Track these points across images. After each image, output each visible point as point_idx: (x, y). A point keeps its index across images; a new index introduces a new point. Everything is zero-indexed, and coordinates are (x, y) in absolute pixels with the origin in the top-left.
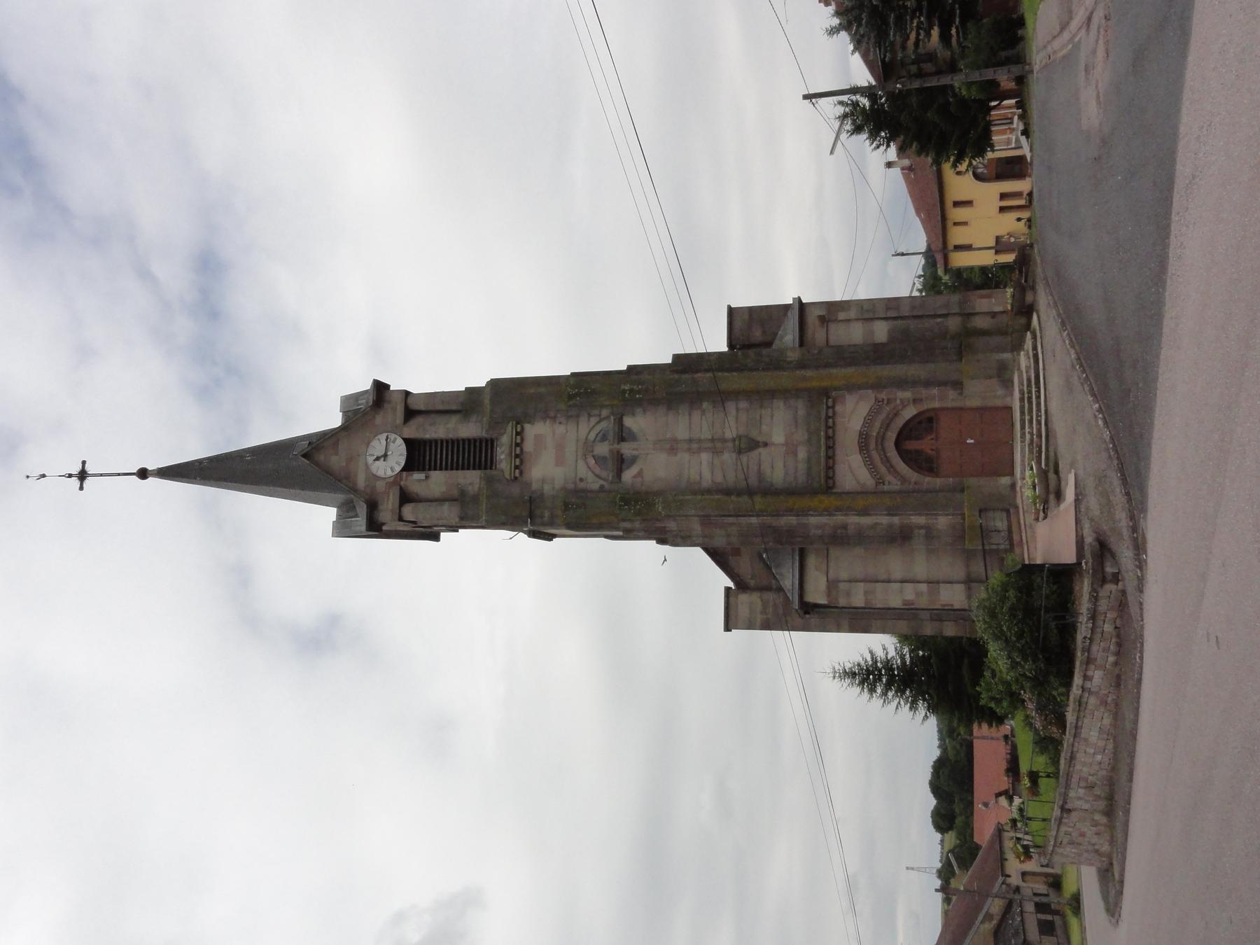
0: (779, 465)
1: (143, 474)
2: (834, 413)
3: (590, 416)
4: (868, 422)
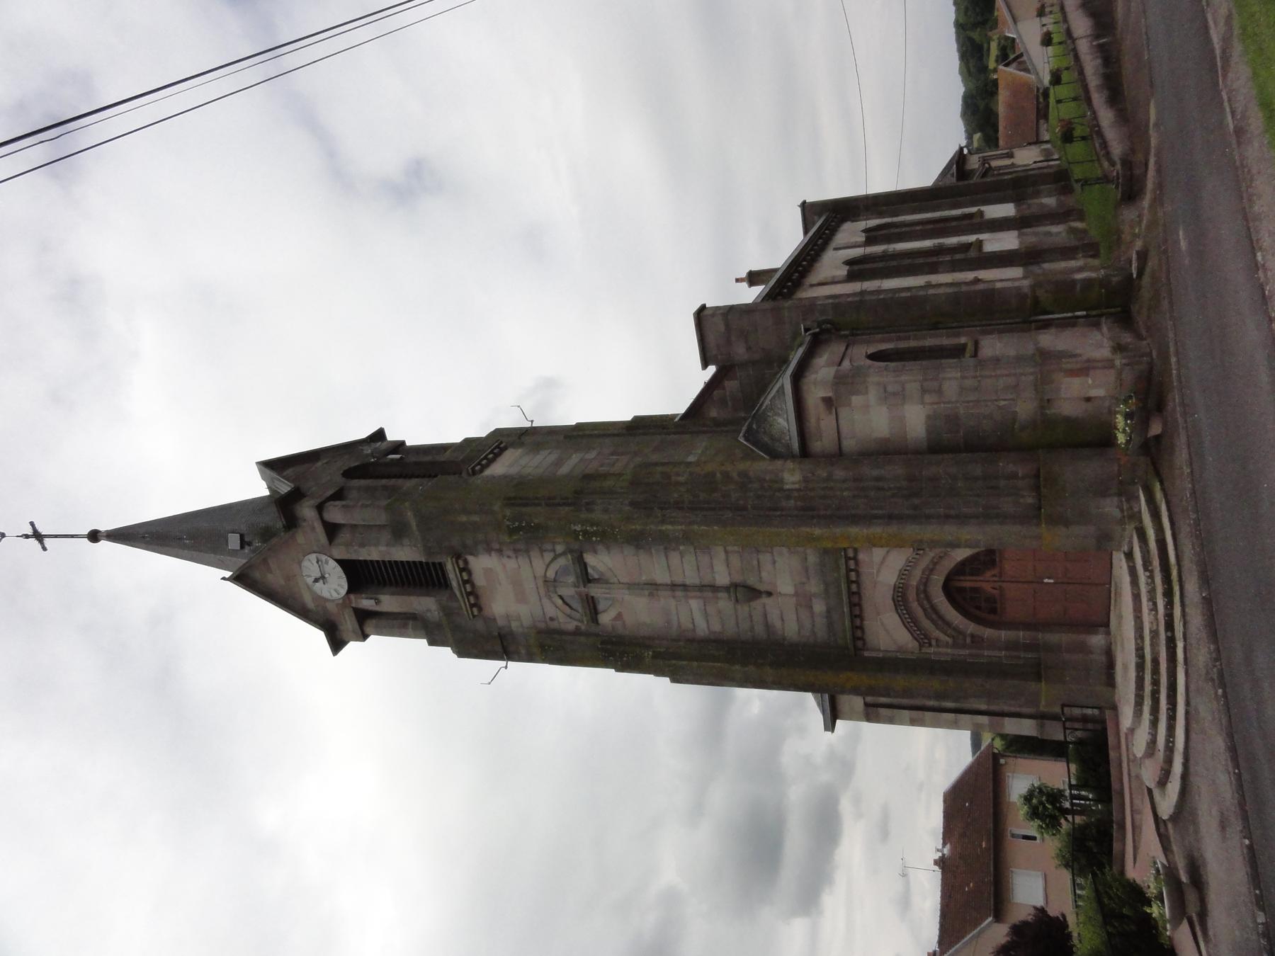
0: (791, 617)
1: (94, 536)
2: (857, 563)
3: (542, 551)
4: (904, 574)
